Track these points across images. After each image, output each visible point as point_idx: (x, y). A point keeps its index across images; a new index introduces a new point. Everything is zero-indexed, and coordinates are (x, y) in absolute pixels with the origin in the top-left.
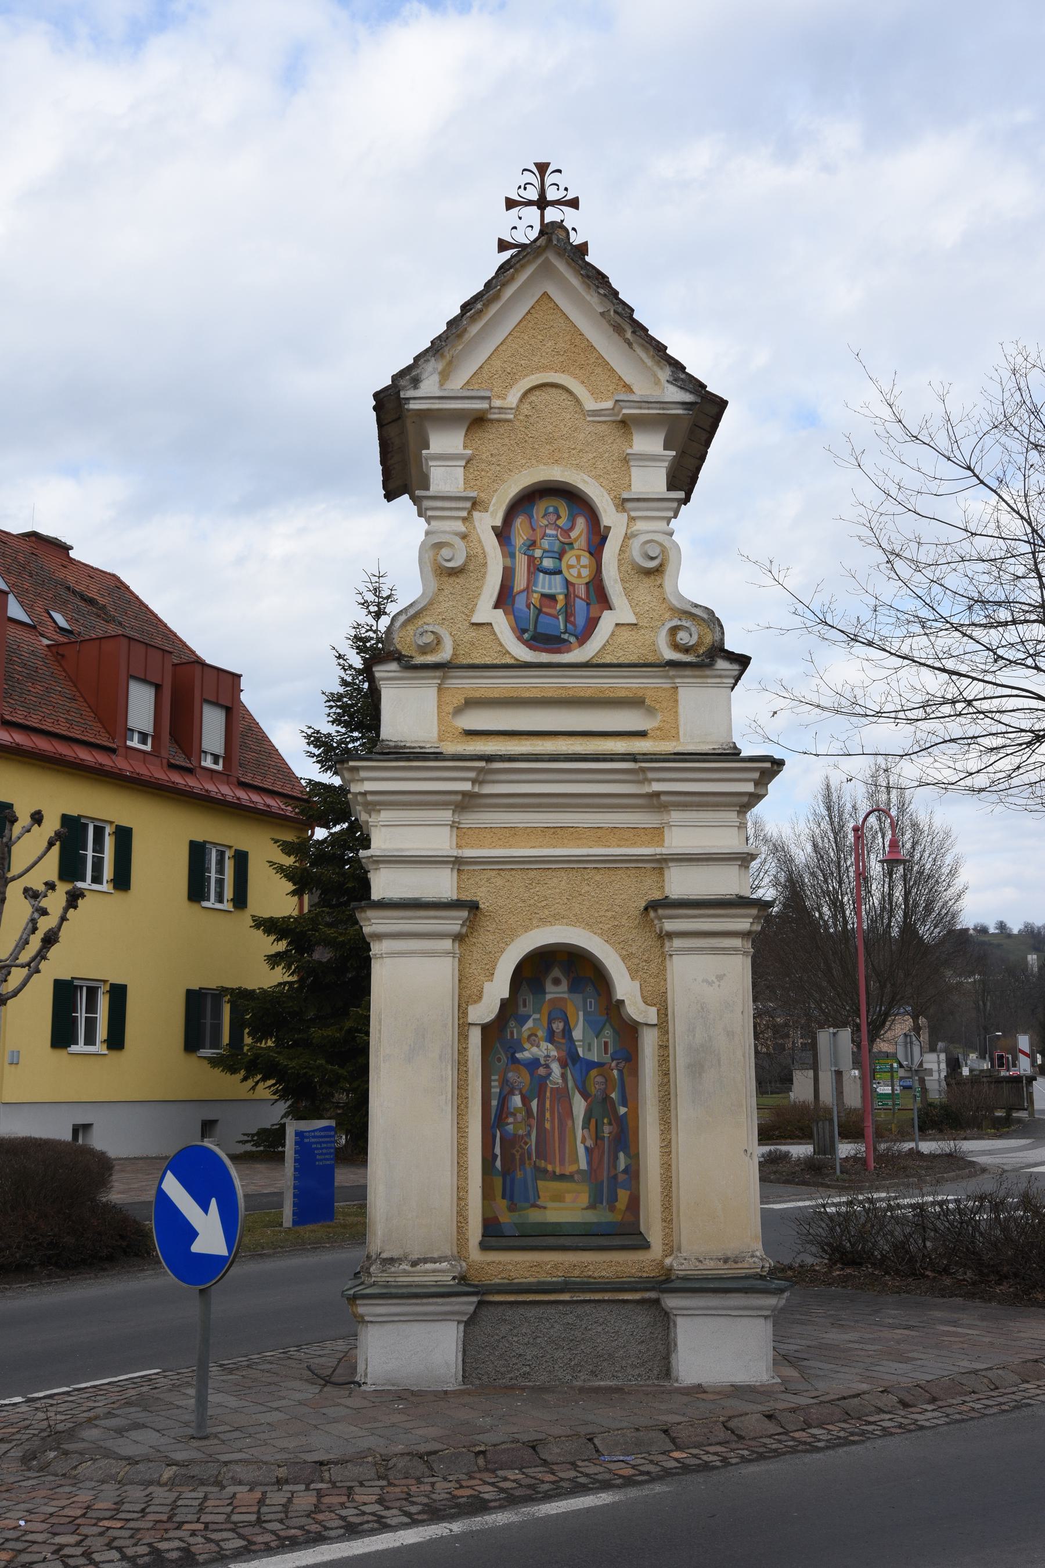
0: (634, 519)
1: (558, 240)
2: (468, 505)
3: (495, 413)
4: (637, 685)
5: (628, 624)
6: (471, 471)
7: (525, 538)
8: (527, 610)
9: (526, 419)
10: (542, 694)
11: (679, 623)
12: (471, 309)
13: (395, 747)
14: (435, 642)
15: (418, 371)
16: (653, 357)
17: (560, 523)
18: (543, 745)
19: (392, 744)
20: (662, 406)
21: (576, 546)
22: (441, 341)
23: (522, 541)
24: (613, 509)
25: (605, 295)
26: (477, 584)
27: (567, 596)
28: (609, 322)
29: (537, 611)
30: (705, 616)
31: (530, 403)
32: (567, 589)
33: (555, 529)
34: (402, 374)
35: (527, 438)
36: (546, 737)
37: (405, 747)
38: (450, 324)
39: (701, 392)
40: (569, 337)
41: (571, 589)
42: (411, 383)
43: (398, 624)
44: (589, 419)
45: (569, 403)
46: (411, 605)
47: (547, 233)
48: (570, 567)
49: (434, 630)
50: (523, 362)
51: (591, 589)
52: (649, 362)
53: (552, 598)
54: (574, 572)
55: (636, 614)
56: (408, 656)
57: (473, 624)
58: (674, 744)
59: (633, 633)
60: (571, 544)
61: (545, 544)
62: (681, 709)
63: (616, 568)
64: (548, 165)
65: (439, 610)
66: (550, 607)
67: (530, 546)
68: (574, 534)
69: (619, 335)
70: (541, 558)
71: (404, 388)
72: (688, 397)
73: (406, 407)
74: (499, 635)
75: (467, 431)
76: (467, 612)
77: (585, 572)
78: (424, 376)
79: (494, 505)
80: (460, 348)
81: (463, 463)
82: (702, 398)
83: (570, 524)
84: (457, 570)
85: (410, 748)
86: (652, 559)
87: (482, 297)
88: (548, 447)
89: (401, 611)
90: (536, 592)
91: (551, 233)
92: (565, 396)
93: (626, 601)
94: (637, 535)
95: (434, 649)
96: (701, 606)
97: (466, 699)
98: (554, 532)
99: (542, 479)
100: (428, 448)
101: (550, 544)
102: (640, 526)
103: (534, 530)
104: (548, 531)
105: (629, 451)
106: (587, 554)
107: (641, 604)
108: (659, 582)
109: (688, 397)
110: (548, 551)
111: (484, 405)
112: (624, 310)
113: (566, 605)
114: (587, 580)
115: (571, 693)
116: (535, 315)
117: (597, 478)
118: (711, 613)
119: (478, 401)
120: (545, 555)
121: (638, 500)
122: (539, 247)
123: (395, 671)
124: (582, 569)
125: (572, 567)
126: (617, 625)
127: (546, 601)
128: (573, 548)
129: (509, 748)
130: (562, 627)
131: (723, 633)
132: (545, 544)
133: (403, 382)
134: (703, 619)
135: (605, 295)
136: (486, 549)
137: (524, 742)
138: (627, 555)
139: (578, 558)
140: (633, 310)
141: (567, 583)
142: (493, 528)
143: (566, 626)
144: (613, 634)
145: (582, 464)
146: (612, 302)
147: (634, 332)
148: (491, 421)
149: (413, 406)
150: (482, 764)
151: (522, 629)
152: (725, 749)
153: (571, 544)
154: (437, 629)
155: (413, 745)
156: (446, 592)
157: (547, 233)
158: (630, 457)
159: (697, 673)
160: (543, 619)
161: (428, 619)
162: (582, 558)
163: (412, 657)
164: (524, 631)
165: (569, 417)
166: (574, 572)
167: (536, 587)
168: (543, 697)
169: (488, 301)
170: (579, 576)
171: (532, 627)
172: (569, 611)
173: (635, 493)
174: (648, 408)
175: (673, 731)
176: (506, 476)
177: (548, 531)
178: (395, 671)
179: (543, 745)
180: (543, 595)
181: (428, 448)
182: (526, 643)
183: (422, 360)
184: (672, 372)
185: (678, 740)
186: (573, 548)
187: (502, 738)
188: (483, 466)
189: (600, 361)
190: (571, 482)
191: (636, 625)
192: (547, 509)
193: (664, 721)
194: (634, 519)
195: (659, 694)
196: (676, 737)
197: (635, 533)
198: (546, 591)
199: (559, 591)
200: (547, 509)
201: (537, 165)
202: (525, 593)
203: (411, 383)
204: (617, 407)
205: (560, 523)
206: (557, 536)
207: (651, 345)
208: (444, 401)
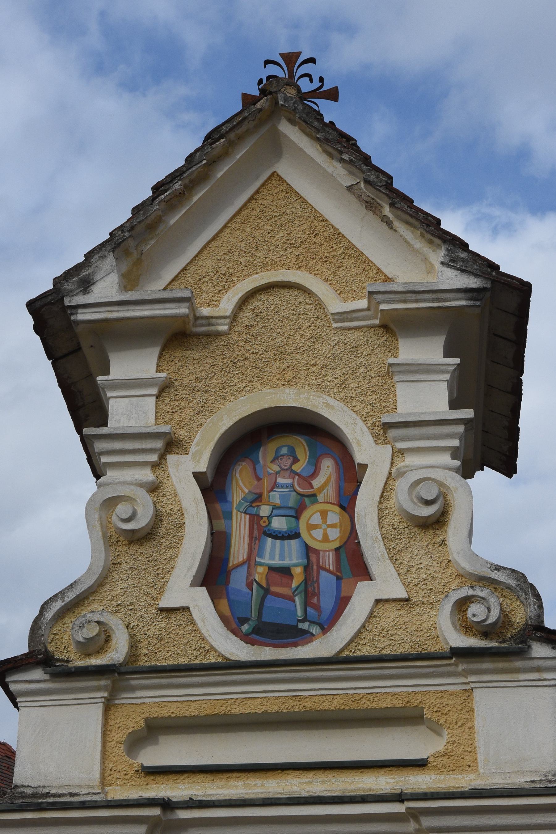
0: (402, 452)
1: (286, 99)
2: (159, 444)
3: (203, 325)
4: (410, 690)
5: (395, 600)
6: (167, 401)
7: (247, 491)
8: (246, 590)
9: (246, 331)
10: (264, 708)
11: (471, 592)
12: (166, 191)
13: (34, 795)
14: (103, 637)
15: (90, 271)
16: (422, 236)
17: (297, 468)
18: (263, 785)
19: (29, 791)
20: (435, 296)
21: (320, 498)
22: (123, 232)
23: (242, 495)
24: (371, 440)
25: (351, 161)
26: (170, 553)
27: (307, 568)
28: (359, 197)
29: (262, 592)
30: (512, 582)
31: (253, 310)
32: (308, 558)
33: (289, 477)
34: (68, 275)
35: (247, 355)
36: (269, 774)
37: (48, 795)
38: (136, 210)
39: (490, 274)
40: (307, 225)
41: (313, 558)
42: (79, 287)
43: (49, 615)
44: (335, 325)
45: (308, 307)
46: (71, 586)
47: (271, 93)
48: (311, 527)
49: (102, 620)
50: (242, 260)
51: (343, 556)
52: (419, 244)
53: (286, 572)
54: (318, 534)
55: (406, 585)
56: (63, 660)
57: (162, 610)
58: (472, 776)
59: (402, 612)
60: (314, 495)
61: (276, 498)
62: (478, 722)
63: (376, 521)
64: (298, 54)
65: (113, 593)
66: (281, 585)
67: (253, 502)
68: (317, 483)
69: (374, 213)
70: (269, 517)
71: (70, 293)
72: (472, 282)
73: (72, 318)
74: (200, 624)
75: (162, 350)
76: (154, 593)
77: (334, 534)
78: (97, 277)
79: (197, 445)
80: (152, 242)
81: (154, 391)
82: (493, 281)
83: (312, 469)
84: (138, 535)
85: (55, 795)
86: (428, 503)
87: (181, 175)
88: (277, 364)
89: (56, 596)
90: (261, 564)
91: (276, 92)
92: (302, 298)
93: (391, 567)
94: (405, 473)
95: (102, 649)
96: (504, 568)
97: (147, 720)
98: (288, 481)
99: (267, 406)
100: (107, 373)
101: (282, 497)
102: (411, 460)
103: (259, 479)
104: (280, 480)
105: (392, 360)
106: (337, 509)
107: (414, 570)
108: (442, 538)
109: (472, 282)
110: (280, 508)
111: (183, 310)
112: (377, 177)
113: (306, 581)
114: (337, 544)
115: (308, 704)
116: (260, 202)
117: (347, 401)
118: (522, 577)
119: (174, 305)
120: (276, 512)
121: (406, 424)
122: (260, 110)
123: (39, 681)
124: (329, 530)
125: (315, 527)
126: (378, 601)
127: (276, 577)
128: (316, 501)
129: (209, 792)
130: (299, 612)
131: (541, 606)
132: (276, 498)
133: (68, 286)
134: (509, 587)
135: (351, 161)
136: (185, 504)
137: (233, 782)
138: (392, 502)
139: (324, 514)
140: (391, 178)
141: (308, 550)
142: (197, 476)
143: (305, 611)
144: (371, 615)
145: (326, 383)
146: (360, 169)
147: (392, 205)
148: (198, 335)
149: (83, 316)
150: (156, 812)
151: (239, 618)
152: (550, 782)
153: (314, 495)
154: (107, 618)
155: (60, 791)
156: (124, 567)
157: (271, 93)
158: (395, 369)
159: (500, 665)
160: (270, 601)
161: (97, 606)
162: (330, 514)
163: (68, 661)
164: (243, 621)
165: (307, 324)
166: (318, 534)
167: (261, 557)
168: (265, 712)
169: (191, 181)
170: (326, 538)
171: (254, 615)
172: (310, 589)
173: (401, 415)
174: (416, 301)
175: (468, 758)
176: (216, 405)
177: (280, 480)
178: (39, 681)
179: (263, 785)
180: (272, 569)
181: (107, 373)
182: (247, 639)
183: (96, 257)
184: (448, 250)
185: (476, 770)
186: (316, 501)
187: (200, 777)
188: (183, 394)
189: (351, 251)
190: (308, 407)
191: (407, 600)
192: (278, 450)
193: (454, 742)
194: (402, 452)
195: (445, 701)
196: (472, 766)
197: (403, 470)
198: (277, 562)
199: (295, 561)
200: (278, 450)
201: (282, 55)
202: (245, 567)
203: (79, 287)
204: (373, 302)
205: (297, 468)
206: (292, 486)
207: (417, 219)
208: (126, 308)
